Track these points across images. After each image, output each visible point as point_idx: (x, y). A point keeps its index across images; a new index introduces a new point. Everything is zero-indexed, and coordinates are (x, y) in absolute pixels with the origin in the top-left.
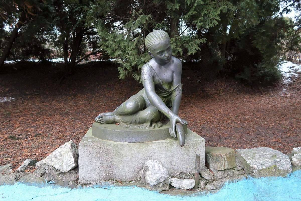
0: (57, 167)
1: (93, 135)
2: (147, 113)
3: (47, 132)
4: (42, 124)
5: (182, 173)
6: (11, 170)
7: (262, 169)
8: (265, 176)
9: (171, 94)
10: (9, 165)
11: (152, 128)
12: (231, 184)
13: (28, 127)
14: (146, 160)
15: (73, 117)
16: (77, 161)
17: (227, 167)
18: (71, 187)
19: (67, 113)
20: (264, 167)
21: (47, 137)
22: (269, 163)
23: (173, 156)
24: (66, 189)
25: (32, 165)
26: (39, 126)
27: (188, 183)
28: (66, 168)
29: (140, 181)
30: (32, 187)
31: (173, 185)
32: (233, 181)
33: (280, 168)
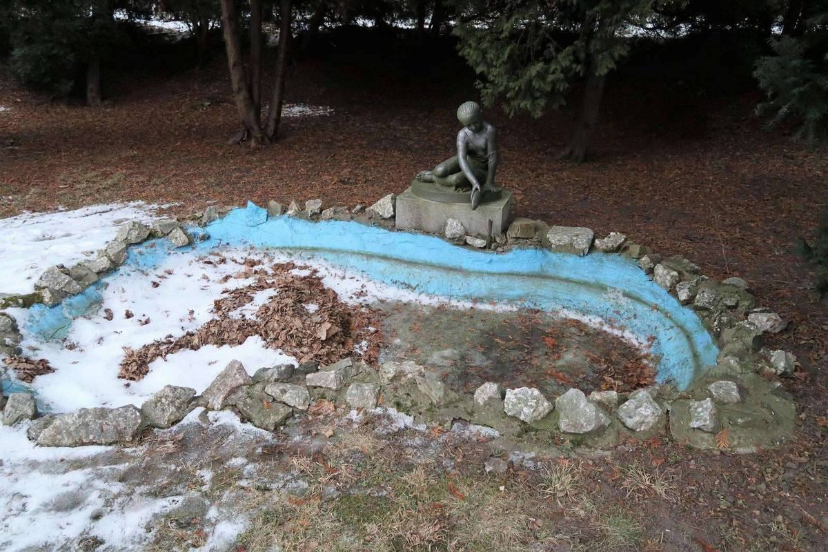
0: (381, 213)
1: (412, 191)
2: (453, 178)
3: (378, 178)
4: (373, 166)
5: (479, 234)
6: (347, 211)
7: (560, 245)
8: (560, 252)
9: (487, 160)
10: (346, 207)
11: (456, 192)
12: (519, 251)
13: (357, 168)
14: (448, 218)
15: (416, 158)
16: (394, 210)
17: (519, 235)
18: (390, 230)
19: (409, 148)
20: (561, 243)
21: (378, 186)
22: (565, 240)
23: (472, 219)
24: (386, 231)
25: (363, 209)
26: (369, 168)
27: (479, 242)
28: (387, 215)
29: (442, 235)
30: (362, 225)
31: (468, 241)
32: (520, 248)
33: (576, 247)
